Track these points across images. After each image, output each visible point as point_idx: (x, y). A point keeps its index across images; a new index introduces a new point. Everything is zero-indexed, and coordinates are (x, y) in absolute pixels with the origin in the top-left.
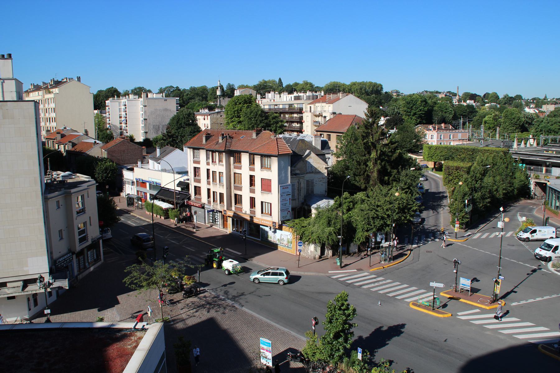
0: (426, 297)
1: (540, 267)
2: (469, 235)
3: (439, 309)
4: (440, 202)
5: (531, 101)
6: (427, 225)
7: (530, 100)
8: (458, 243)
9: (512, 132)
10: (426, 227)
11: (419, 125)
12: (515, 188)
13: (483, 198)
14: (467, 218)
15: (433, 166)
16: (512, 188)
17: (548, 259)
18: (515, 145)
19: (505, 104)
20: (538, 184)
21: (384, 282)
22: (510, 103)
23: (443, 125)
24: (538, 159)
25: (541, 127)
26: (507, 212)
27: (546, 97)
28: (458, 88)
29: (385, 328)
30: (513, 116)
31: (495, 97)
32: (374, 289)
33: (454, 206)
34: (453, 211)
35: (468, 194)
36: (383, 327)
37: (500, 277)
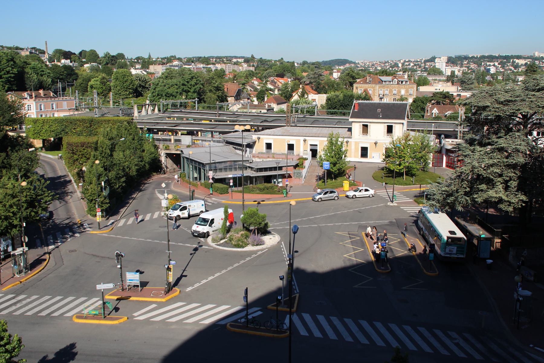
0: (92, 304)
1: (200, 244)
2: (113, 223)
3: (110, 315)
4: (64, 189)
5: (136, 61)
6: (58, 219)
7: (134, 60)
8: (104, 235)
9: (125, 98)
10: (57, 222)
11: (9, 93)
12: (146, 163)
13: (118, 178)
14: (107, 203)
15: (41, 145)
16: (143, 162)
17: (206, 235)
18: (136, 114)
19: (107, 64)
20: (168, 155)
21: (28, 300)
22: (112, 63)
23: (41, 92)
24: (166, 127)
25: (158, 91)
26: (143, 190)
27: (150, 56)
28: (46, 44)
29: (51, 356)
30: (125, 79)
31: (93, 56)
32: (18, 312)
33: (90, 191)
34: (89, 197)
35: (104, 175)
36: (47, 356)
37: (171, 262)
